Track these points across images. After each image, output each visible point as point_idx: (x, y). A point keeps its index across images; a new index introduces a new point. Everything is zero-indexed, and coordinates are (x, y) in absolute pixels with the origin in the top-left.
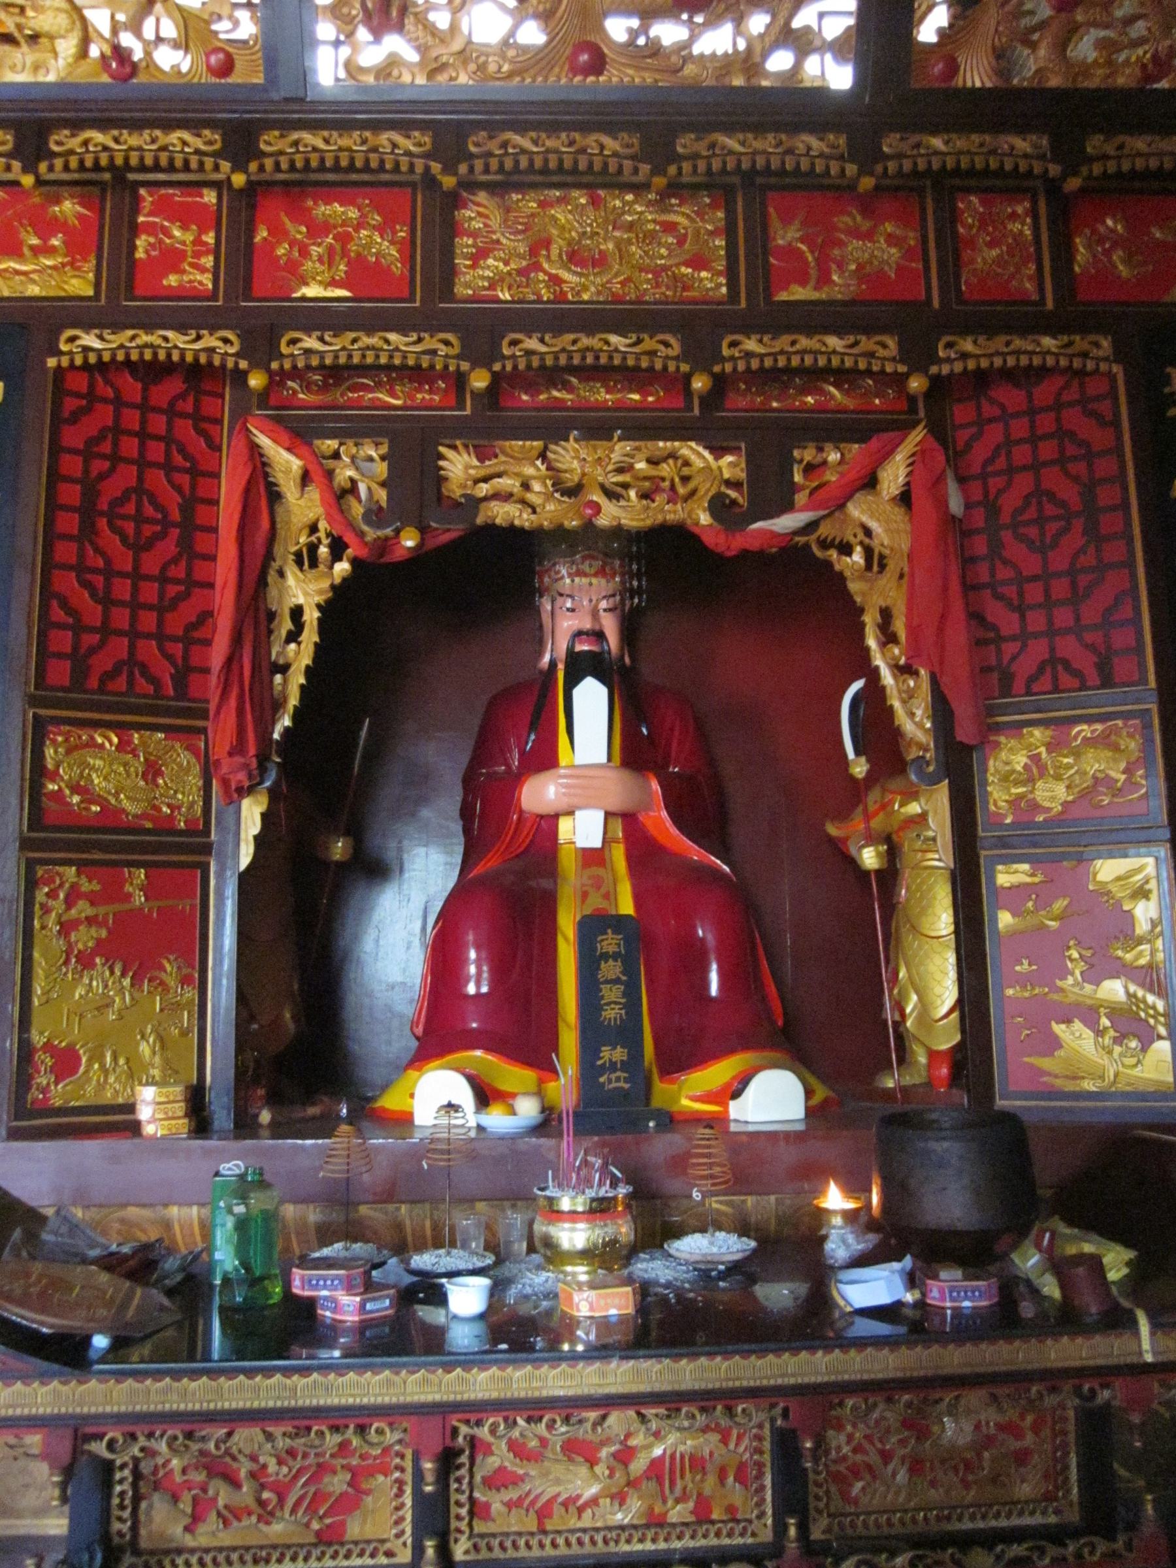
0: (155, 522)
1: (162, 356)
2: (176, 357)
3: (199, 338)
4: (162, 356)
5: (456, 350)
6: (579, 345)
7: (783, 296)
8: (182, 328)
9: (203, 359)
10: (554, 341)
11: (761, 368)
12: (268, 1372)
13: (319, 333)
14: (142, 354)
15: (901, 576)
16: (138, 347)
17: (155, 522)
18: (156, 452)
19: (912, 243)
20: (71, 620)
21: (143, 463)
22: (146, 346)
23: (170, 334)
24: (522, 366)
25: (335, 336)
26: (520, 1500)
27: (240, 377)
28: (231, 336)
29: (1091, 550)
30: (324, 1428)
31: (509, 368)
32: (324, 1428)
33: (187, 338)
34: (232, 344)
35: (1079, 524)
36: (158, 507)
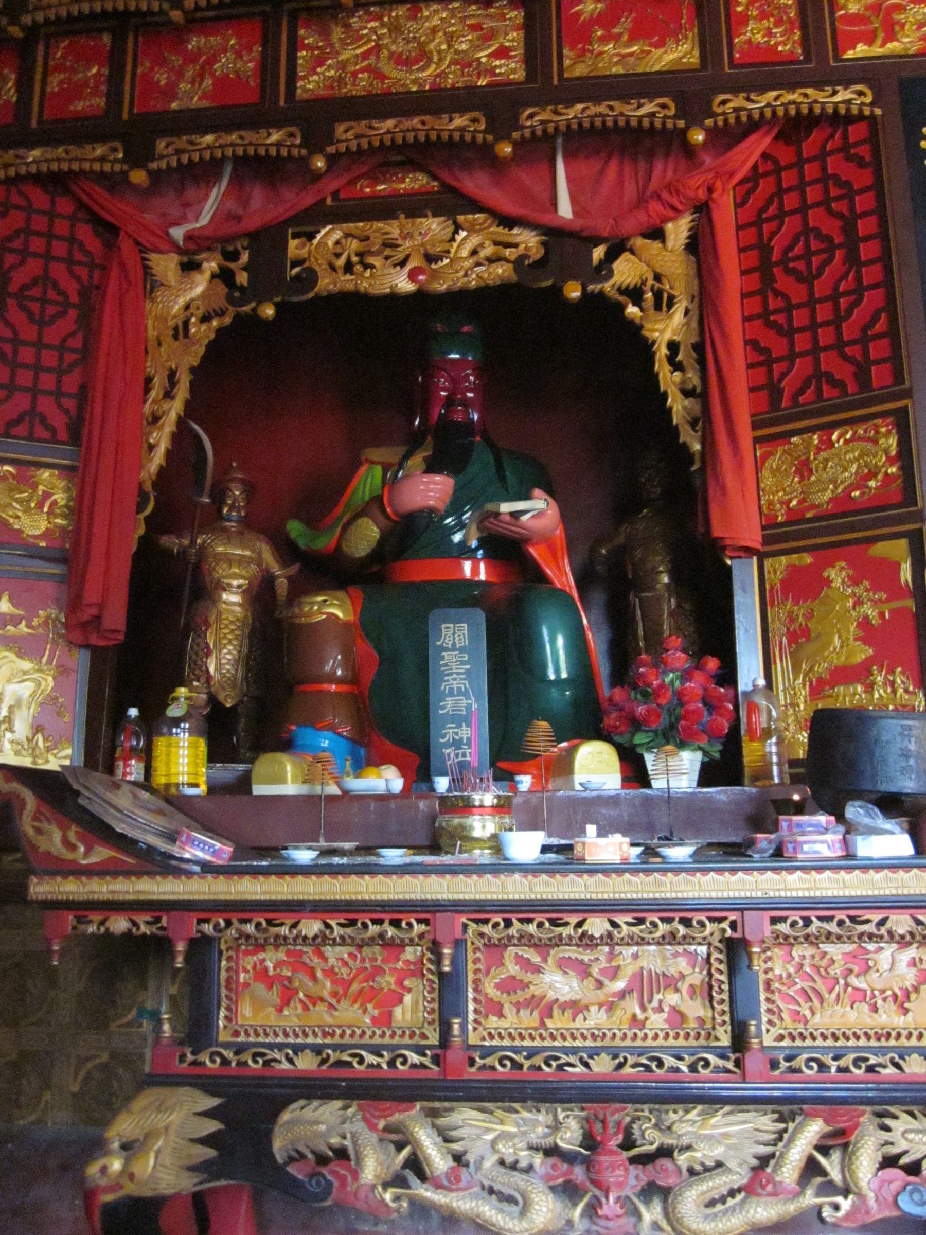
0: (807, 242)
1: (805, 110)
2: (817, 110)
3: (835, 93)
4: (805, 110)
5: (672, 112)
6: (588, 112)
7: (850, 54)
8: (819, 86)
9: (646, 123)
10: (759, 98)
11: (28, 173)
12: (734, 871)
13: (745, 95)
14: (786, 111)
15: (693, 297)
16: (782, 104)
17: (807, 242)
18: (59, 248)
19: (792, 15)
20: (771, 318)
21: (47, 256)
22: (790, 103)
23: (809, 91)
24: (732, 121)
25: (567, 108)
26: (46, 1107)
27: (304, 163)
28: (530, 111)
29: (80, 336)
30: (704, 919)
31: (720, 123)
32: (704, 919)
33: (630, 107)
34: (669, 109)
35: (73, 314)
36: (61, 293)
